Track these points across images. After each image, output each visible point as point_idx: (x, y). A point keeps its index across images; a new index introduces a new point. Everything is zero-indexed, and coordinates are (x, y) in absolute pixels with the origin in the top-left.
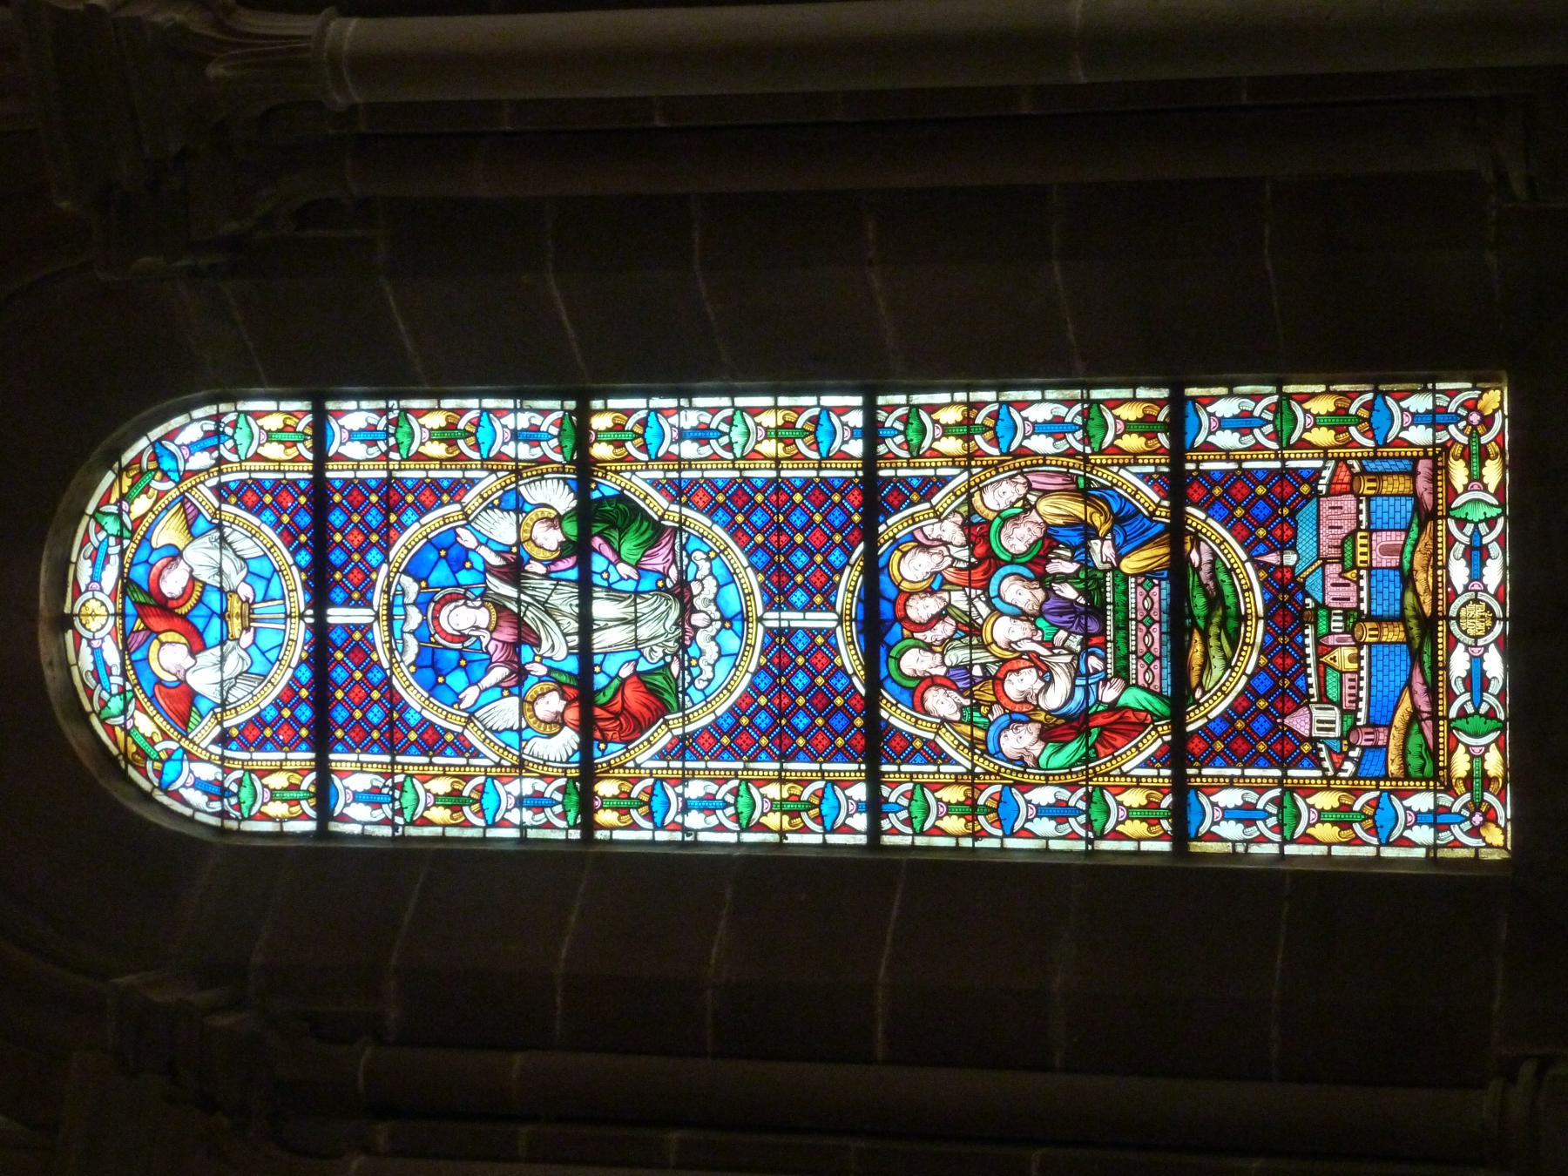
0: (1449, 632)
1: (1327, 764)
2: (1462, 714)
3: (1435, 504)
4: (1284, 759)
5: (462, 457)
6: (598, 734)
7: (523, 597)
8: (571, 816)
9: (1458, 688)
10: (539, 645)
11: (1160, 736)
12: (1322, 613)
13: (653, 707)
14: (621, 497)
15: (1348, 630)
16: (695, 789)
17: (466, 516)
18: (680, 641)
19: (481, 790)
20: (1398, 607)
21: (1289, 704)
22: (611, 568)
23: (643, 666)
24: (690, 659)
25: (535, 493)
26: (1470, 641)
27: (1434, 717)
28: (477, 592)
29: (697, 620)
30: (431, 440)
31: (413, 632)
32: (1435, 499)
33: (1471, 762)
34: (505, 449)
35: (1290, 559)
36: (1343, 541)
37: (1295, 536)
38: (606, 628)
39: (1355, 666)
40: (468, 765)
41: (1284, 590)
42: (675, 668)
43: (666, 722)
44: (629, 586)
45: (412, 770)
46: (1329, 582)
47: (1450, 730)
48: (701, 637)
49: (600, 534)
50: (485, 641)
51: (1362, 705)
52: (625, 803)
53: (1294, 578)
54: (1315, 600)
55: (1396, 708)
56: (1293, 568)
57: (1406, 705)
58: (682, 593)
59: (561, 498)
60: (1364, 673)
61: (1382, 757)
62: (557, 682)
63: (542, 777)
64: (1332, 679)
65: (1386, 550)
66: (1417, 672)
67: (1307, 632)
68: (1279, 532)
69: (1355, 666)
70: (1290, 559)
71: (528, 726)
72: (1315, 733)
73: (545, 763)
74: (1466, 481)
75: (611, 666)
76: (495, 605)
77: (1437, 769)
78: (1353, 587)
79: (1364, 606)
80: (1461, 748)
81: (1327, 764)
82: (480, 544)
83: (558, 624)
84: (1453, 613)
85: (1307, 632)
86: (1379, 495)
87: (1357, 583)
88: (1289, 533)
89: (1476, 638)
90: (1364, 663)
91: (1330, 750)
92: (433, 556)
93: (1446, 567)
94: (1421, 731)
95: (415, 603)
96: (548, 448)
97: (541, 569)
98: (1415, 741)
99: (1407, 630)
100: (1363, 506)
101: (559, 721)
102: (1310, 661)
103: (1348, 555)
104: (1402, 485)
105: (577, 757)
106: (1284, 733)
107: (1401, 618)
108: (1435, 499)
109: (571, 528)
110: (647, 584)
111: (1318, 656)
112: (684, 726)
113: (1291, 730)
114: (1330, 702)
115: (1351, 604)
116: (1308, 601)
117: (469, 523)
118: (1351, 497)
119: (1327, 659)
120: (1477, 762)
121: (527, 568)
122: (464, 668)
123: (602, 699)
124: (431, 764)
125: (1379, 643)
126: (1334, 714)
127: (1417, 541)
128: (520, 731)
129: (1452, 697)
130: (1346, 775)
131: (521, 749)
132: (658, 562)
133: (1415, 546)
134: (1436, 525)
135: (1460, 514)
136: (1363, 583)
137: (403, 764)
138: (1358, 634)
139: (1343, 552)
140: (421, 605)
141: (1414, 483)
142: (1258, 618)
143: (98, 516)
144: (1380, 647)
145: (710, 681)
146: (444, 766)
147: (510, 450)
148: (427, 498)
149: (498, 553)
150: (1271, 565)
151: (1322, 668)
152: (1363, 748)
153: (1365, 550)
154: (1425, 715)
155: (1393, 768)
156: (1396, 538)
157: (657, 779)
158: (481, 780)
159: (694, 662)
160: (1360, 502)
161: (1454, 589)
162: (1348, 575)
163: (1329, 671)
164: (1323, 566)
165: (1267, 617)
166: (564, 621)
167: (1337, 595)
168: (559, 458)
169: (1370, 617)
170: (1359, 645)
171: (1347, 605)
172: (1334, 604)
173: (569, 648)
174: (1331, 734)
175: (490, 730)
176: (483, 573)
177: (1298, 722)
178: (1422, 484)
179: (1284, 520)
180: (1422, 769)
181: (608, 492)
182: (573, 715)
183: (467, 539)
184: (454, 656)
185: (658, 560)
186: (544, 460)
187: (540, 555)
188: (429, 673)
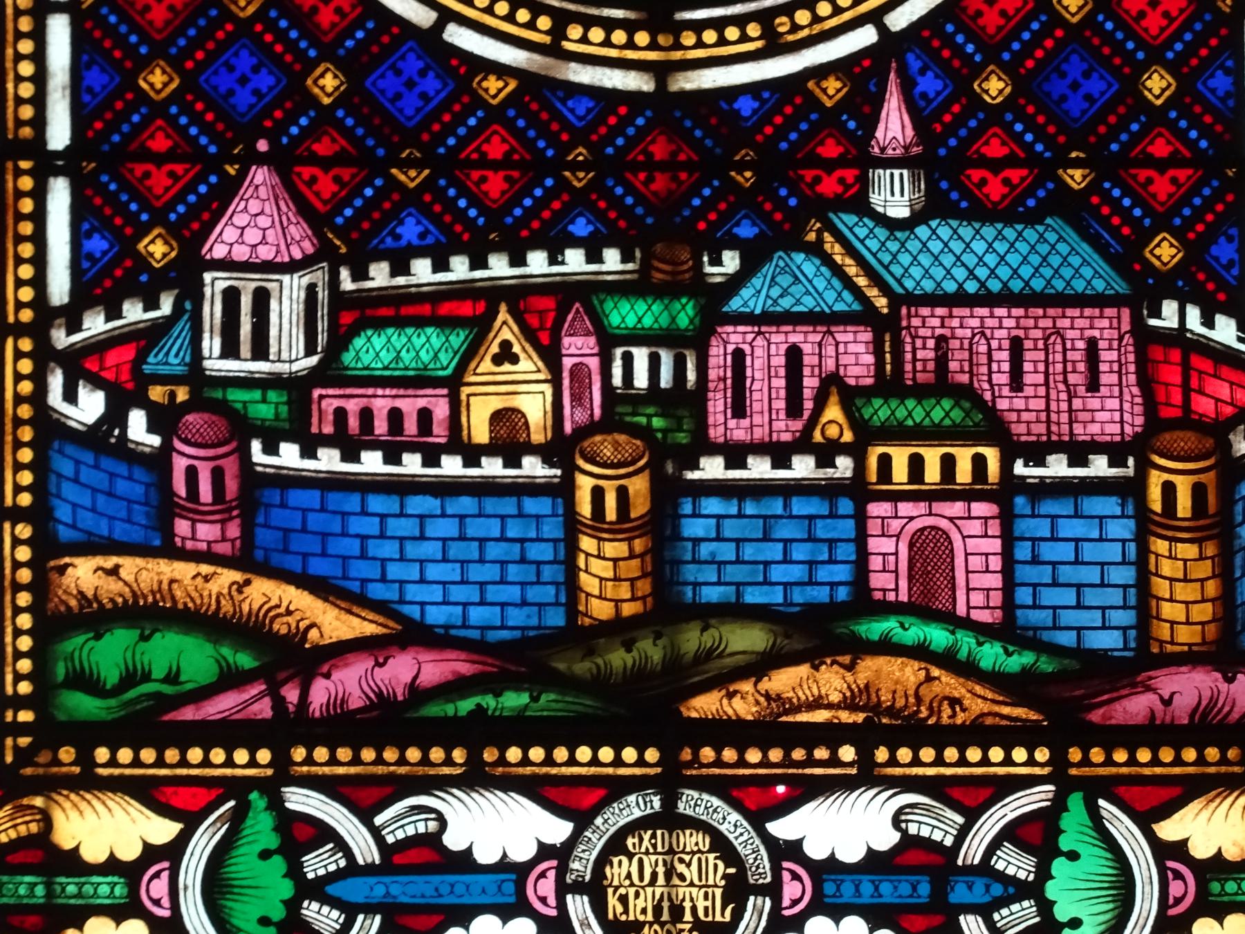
0: (617, 788)
1: (95, 324)
2: (301, 835)
3: (1114, 736)
4: (115, 161)
9: (400, 820)
12: (685, 314)
15: (619, 408)
20: (712, 594)
21: (326, 186)
26: (581, 865)
27: (288, 729)
32: (1131, 736)
33: (112, 865)
35: (894, 195)
36: (966, 394)
37: (980, 213)
39: (480, 433)
41: (773, 168)
46: (806, 339)
47: (237, 788)
51: (329, 460)
53: (822, 208)
54: (735, 283)
55: (320, 588)
56: (862, 207)
57: (334, 624)
60: (452, 466)
61: (121, 532)
64: (429, 347)
65: (930, 553)
66: (458, 665)
67: (612, 259)
68: (160, 143)
69: (480, 433)
70: (894, 195)
72: (215, 283)
74: (1201, 850)
77: (86, 736)
78: (786, 430)
79: (712, 468)
80: (163, 830)
81: (95, 324)
84: (693, 802)
85: (612, 259)
86: (1146, 526)
87: (803, 444)
88: (995, 190)
89: (595, 890)
90: (492, 467)
91: (153, 334)
93: (867, 776)
94: (229, 679)
98: (194, 657)
99: (620, 629)
100: (1099, 466)
102: (499, 266)
103: (913, 412)
104: (1184, 611)
106: (214, 165)
107: (667, 605)
108: (1131, 736)
111: (517, 296)
113: (227, 192)
114: (340, 340)
115: (720, 420)
116: (731, 262)
118: (1135, 422)
119: (506, 329)
120: (108, 889)
125: (573, 526)
126: (291, 353)
127: (967, 669)
129: (364, 797)
130: (55, 397)
133: (947, 660)
134: (1027, 736)
135: (1073, 829)
136: (803, 467)
138: (605, 446)
139: (921, 392)
141: (1191, 658)
142: (660, 71)
144: (553, 528)
150: (871, 121)
151: (468, 311)
152: (160, 461)
153: (932, 473)
154: (291, 695)
155: (83, 574)
156: (977, 582)
160: (1116, 454)
161: (785, 807)
162: (833, 412)
163: (458, 339)
164: (865, 316)
165: (665, 107)
167: (755, 368)
169: (671, 493)
170: (560, 449)
171: (717, 405)
172: (718, 356)
174: (211, 344)
177: (254, 223)
178: (1187, 688)
179: (1047, 170)
180: (86, 682)
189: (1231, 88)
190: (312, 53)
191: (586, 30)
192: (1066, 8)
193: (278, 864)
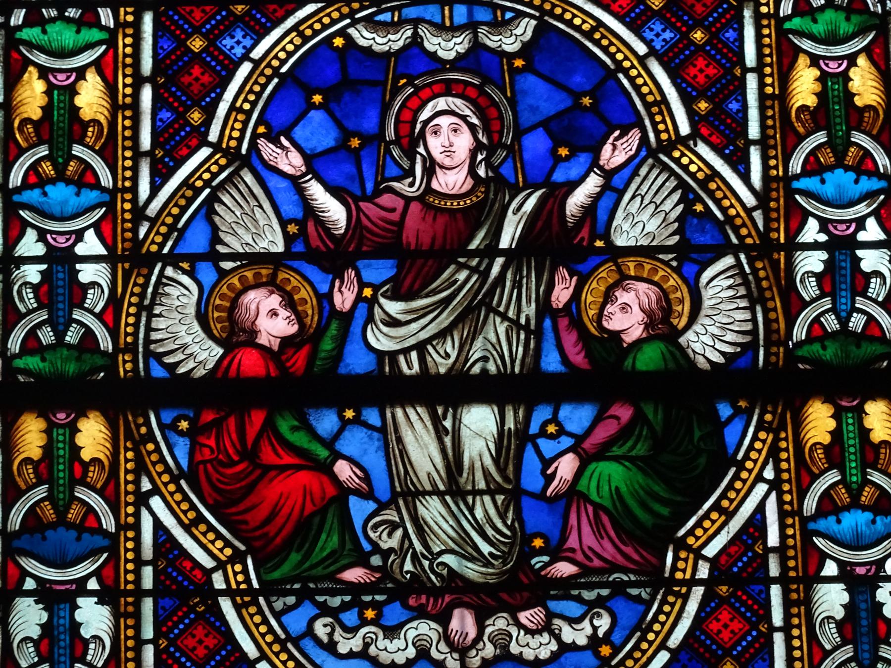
5: (792, 141)
6: (208, 416)
7: (500, 261)
8: (33, 362)
10: (394, 297)
11: (221, 565)
13: (271, 529)
14: (723, 460)
16: (93, 617)
17: (667, 147)
18: (417, 584)
19: (85, 179)
22: (566, 442)
23: (359, 509)
24: (376, 606)
25: (718, 283)
28: (507, 171)
29: (463, 622)
30: (823, 79)
31: (416, 42)
34: (812, 225)
38: (440, 432)
40: (138, 155)
42: (354, 575)
43: (238, 557)
44: (532, 480)
45: (124, 42)
48: (426, 628)
49: (639, 418)
50: (401, 186)
52: (61, 472)
58: (516, 587)
59: (708, 341)
62: (321, 330)
63: (114, 302)
71: (223, 274)
73: (147, 309)
75: (354, 442)
76: (479, 207)
82: (608, 175)
83: (442, 335)
92: (578, 80)
95: (477, 46)
96: (817, 311)
97: (561, 295)
101: (235, 334)
105: (158, 372)
109: (649, 358)
110: (538, 518)
112: (228, 592)
117: (653, 153)
121: (563, 272)
122: (342, 146)
123: (284, 426)
124: (138, 81)
128: (214, 257)
131: (173, 260)
132: (583, 535)
137: (137, 25)
140: (477, 58)
143: (106, 198)
145: (331, 647)
146: (135, 106)
147: (811, 232)
148: (702, 70)
149: (589, 210)
157: (113, 539)
158: (106, 178)
159: (370, 614)
166: (450, 347)
168: (800, 332)
173: (393, 355)
175: (213, 198)
176: (546, 182)
181: (731, 434)
182: (250, 363)
183: (615, 153)
184: (369, 124)
185: (589, 540)
186: (794, 304)
187: (591, 297)
188: (331, 73)
189: (160, 40)
190: (754, 633)
191: (580, 26)
192: (732, 664)
193: (827, 176)
